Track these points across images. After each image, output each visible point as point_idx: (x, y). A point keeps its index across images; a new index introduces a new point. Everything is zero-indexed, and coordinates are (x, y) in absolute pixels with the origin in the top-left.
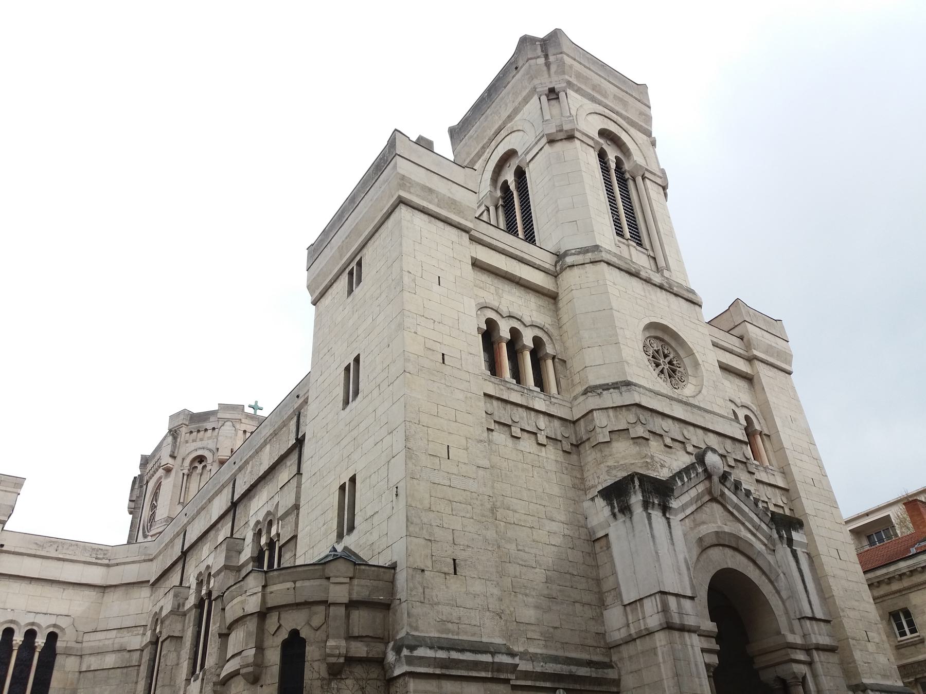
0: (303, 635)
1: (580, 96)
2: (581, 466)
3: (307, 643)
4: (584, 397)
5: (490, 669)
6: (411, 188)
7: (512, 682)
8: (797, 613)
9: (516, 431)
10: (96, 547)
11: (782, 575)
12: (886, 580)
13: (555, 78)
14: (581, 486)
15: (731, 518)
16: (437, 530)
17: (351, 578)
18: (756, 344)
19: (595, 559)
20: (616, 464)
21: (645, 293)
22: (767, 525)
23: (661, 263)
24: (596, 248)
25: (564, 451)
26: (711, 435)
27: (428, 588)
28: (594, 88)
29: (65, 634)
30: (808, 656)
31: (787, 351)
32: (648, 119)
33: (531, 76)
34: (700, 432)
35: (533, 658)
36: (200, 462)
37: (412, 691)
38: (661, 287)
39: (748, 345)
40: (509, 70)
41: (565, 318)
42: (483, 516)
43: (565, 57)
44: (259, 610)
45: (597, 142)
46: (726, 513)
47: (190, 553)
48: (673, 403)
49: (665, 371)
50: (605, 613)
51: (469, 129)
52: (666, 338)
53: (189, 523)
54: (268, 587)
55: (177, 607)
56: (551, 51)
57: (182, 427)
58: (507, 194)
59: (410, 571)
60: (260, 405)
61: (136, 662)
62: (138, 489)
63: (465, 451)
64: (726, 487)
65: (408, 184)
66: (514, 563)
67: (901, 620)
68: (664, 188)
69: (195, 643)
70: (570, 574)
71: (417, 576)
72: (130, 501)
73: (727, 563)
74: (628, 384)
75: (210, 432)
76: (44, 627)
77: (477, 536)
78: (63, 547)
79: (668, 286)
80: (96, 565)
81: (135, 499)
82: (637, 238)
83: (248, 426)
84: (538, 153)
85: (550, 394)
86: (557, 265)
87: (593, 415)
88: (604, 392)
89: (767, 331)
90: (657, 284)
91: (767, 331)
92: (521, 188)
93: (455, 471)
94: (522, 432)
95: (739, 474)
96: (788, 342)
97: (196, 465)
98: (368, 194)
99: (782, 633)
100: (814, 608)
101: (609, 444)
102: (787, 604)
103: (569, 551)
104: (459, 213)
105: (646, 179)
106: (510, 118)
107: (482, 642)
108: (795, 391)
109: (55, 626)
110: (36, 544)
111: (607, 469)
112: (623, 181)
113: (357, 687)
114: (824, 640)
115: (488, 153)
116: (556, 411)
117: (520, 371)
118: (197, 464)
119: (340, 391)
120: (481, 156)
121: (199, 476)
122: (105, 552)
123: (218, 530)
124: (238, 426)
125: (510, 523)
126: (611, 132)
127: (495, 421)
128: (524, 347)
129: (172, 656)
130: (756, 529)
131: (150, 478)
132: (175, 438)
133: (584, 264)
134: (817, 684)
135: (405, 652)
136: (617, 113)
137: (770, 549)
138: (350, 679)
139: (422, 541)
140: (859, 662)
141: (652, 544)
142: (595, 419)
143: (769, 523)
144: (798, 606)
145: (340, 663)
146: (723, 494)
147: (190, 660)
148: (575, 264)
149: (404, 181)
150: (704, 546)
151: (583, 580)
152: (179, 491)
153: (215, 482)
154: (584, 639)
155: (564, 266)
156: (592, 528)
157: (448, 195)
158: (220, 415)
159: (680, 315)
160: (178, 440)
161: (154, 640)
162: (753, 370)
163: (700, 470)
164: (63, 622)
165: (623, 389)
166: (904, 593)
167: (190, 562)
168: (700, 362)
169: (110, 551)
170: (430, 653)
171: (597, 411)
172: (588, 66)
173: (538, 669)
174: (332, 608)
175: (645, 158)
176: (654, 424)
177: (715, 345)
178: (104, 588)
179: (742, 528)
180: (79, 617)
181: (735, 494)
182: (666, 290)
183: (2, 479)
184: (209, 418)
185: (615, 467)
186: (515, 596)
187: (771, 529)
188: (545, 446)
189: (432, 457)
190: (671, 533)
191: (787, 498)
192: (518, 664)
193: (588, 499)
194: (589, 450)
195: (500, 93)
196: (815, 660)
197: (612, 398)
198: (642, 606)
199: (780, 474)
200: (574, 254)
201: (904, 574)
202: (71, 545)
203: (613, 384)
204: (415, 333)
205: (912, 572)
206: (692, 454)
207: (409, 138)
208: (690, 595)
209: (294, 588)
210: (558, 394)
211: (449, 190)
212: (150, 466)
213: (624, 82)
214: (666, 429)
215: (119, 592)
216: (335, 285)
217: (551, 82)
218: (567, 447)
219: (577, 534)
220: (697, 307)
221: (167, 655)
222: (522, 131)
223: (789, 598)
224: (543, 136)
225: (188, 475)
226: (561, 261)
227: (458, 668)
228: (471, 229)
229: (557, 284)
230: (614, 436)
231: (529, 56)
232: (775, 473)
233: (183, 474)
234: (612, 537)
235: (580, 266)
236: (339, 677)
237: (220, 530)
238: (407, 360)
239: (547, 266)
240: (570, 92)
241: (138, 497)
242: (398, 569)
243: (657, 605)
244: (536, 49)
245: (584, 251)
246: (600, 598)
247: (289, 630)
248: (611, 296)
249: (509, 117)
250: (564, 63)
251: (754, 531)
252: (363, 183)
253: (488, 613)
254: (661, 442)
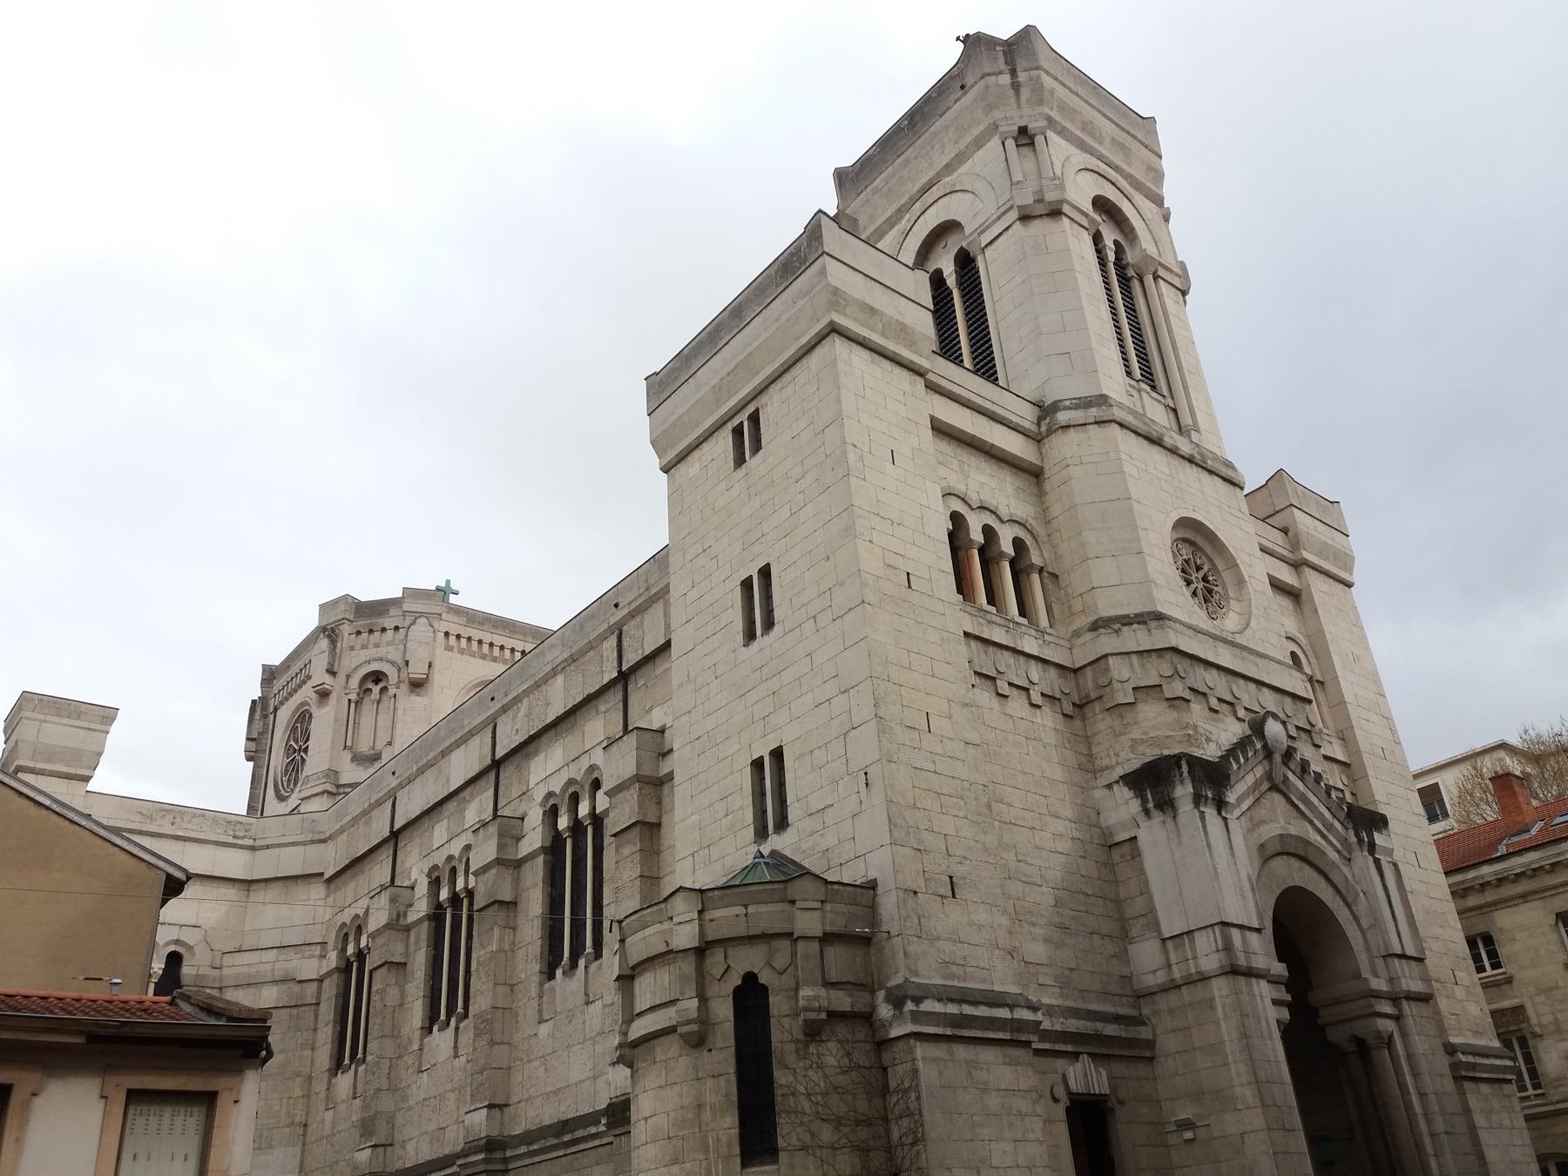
0: (763, 979)
1: (1064, 142)
2: (1087, 737)
3: (770, 992)
4: (1092, 635)
5: (1009, 1029)
6: (847, 308)
7: (1034, 1046)
8: (1382, 947)
9: (1003, 686)
10: (233, 818)
11: (1362, 895)
12: (1460, 891)
13: (1027, 110)
14: (1088, 766)
15: (1296, 814)
16: (926, 835)
17: (822, 902)
18: (1306, 541)
19: (1113, 872)
20: (1143, 737)
21: (1170, 470)
22: (1342, 823)
23: (1186, 420)
24: (1103, 400)
25: (1065, 715)
26: (1266, 691)
27: (924, 916)
29: (194, 954)
30: (1395, 1007)
31: (1347, 552)
32: (1159, 176)
33: (990, 105)
34: (1252, 686)
35: (1050, 1011)
36: (377, 682)
37: (920, 1059)
38: (1191, 460)
39: (1295, 544)
40: (948, 89)
41: (1056, 509)
42: (979, 814)
43: (1044, 76)
44: (697, 945)
45: (1092, 221)
46: (1289, 807)
47: (406, 834)
48: (1219, 644)
49: (1199, 592)
50: (1130, 947)
51: (874, 176)
52: (1199, 541)
53: (401, 786)
54: (706, 913)
55: (395, 917)
56: (1021, 64)
57: (344, 623)
58: (940, 292)
59: (901, 893)
60: (454, 586)
61: (312, 998)
62: (260, 720)
63: (948, 720)
64: (1290, 769)
65: (842, 302)
66: (1015, 878)
67: (1479, 949)
68: (1184, 293)
69: (431, 973)
70: (1084, 893)
71: (910, 900)
72: (248, 739)
73: (1293, 878)
74: (1159, 617)
75: (390, 633)
76: (161, 944)
77: (974, 843)
78: (183, 819)
79: (1199, 458)
80: (234, 847)
81: (255, 736)
82: (1148, 376)
83: (452, 625)
84: (1001, 234)
85: (1038, 627)
86: (1042, 423)
87: (1107, 663)
88: (1125, 629)
89: (1321, 521)
91: (1321, 521)
92: (965, 285)
93: (939, 749)
94: (1011, 688)
95: (1304, 751)
96: (1348, 536)
97: (370, 687)
98: (769, 308)
99: (1364, 976)
100: (1404, 940)
101: (1133, 706)
102: (1369, 936)
103: (1081, 861)
104: (910, 345)
105: (1160, 280)
106: (949, 168)
107: (993, 991)
108: (1357, 615)
109: (177, 942)
110: (141, 813)
111: (1130, 744)
112: (1125, 281)
113: (842, 1052)
114: (1416, 986)
115: (908, 221)
116: (1051, 654)
118: (370, 686)
119: (736, 616)
120: (895, 224)
121: (375, 704)
122: (247, 827)
123: (465, 801)
124: (436, 625)
125: (1006, 823)
126: (1108, 201)
127: (975, 672)
128: (1002, 554)
129: (393, 995)
131: (282, 703)
132: (333, 642)
133: (1085, 424)
134: (1406, 1046)
135: (910, 1006)
136: (1117, 169)
137: (1345, 858)
138: (833, 1041)
139: (909, 852)
140: (1446, 1014)
141: (1207, 854)
142: (1112, 668)
144: (1383, 938)
145: (821, 1020)
146: (1286, 779)
147: (426, 999)
148: (1072, 423)
149: (837, 298)
150: (1267, 854)
151: (1100, 902)
152: (344, 728)
153: (454, 725)
154: (1107, 984)
155: (1055, 427)
156: (1108, 827)
157: (896, 317)
158: (407, 607)
159: (1217, 503)
160: (339, 645)
161: (343, 965)
162: (1300, 581)
163: (1259, 746)
164: (190, 937)
165: (1153, 624)
166: (1485, 910)
167: (408, 848)
168: (1247, 579)
169: (254, 826)
170: (937, 1007)
171: (1114, 657)
172: (1075, 90)
173: (1058, 1027)
174: (801, 945)
175: (1156, 243)
176: (1196, 678)
177: (1263, 550)
178: (248, 884)
179: (1309, 828)
180: (212, 928)
181: (1301, 779)
182: (1197, 465)
183: (82, 710)
184: (388, 610)
185: (1143, 741)
186: (1020, 926)
187: (1347, 829)
188: (1039, 707)
189: (909, 730)
190: (1229, 838)
191: (1348, 777)
192: (1041, 1022)
193: (1100, 785)
194: (1101, 712)
195: (931, 123)
196: (1405, 1013)
197: (1136, 638)
198: (1192, 941)
199: (1338, 741)
200: (1070, 408)
201: (1488, 883)
202: (195, 816)
203: (1137, 615)
204: (871, 542)
205: (1501, 881)
206: (1244, 721)
207: (840, 227)
208: (1257, 927)
209: (746, 915)
210: (1050, 627)
211: (896, 307)
212: (278, 684)
213: (1125, 115)
214: (1211, 685)
215: (273, 892)
216: (706, 447)
217: (1022, 117)
218: (1069, 709)
219: (1088, 836)
220: (1238, 490)
221: (384, 990)
222: (971, 192)
223: (1371, 926)
224: (1011, 207)
225: (357, 703)
226: (1048, 418)
227: (971, 1028)
228: (928, 371)
229: (1041, 453)
230: (1139, 695)
231: (987, 70)
232: (1332, 740)
233: (349, 700)
234: (1144, 842)
235: (1079, 428)
236: (818, 1039)
237: (468, 801)
238: (864, 585)
239: (1027, 425)
240: (1051, 134)
241: (260, 734)
242: (880, 890)
243: (1216, 941)
244: (996, 59)
245: (1085, 403)
246: (1122, 928)
247: (742, 973)
248: (1128, 477)
249: (947, 166)
250: (1043, 86)
252: (758, 288)
253: (997, 951)
254: (1205, 704)
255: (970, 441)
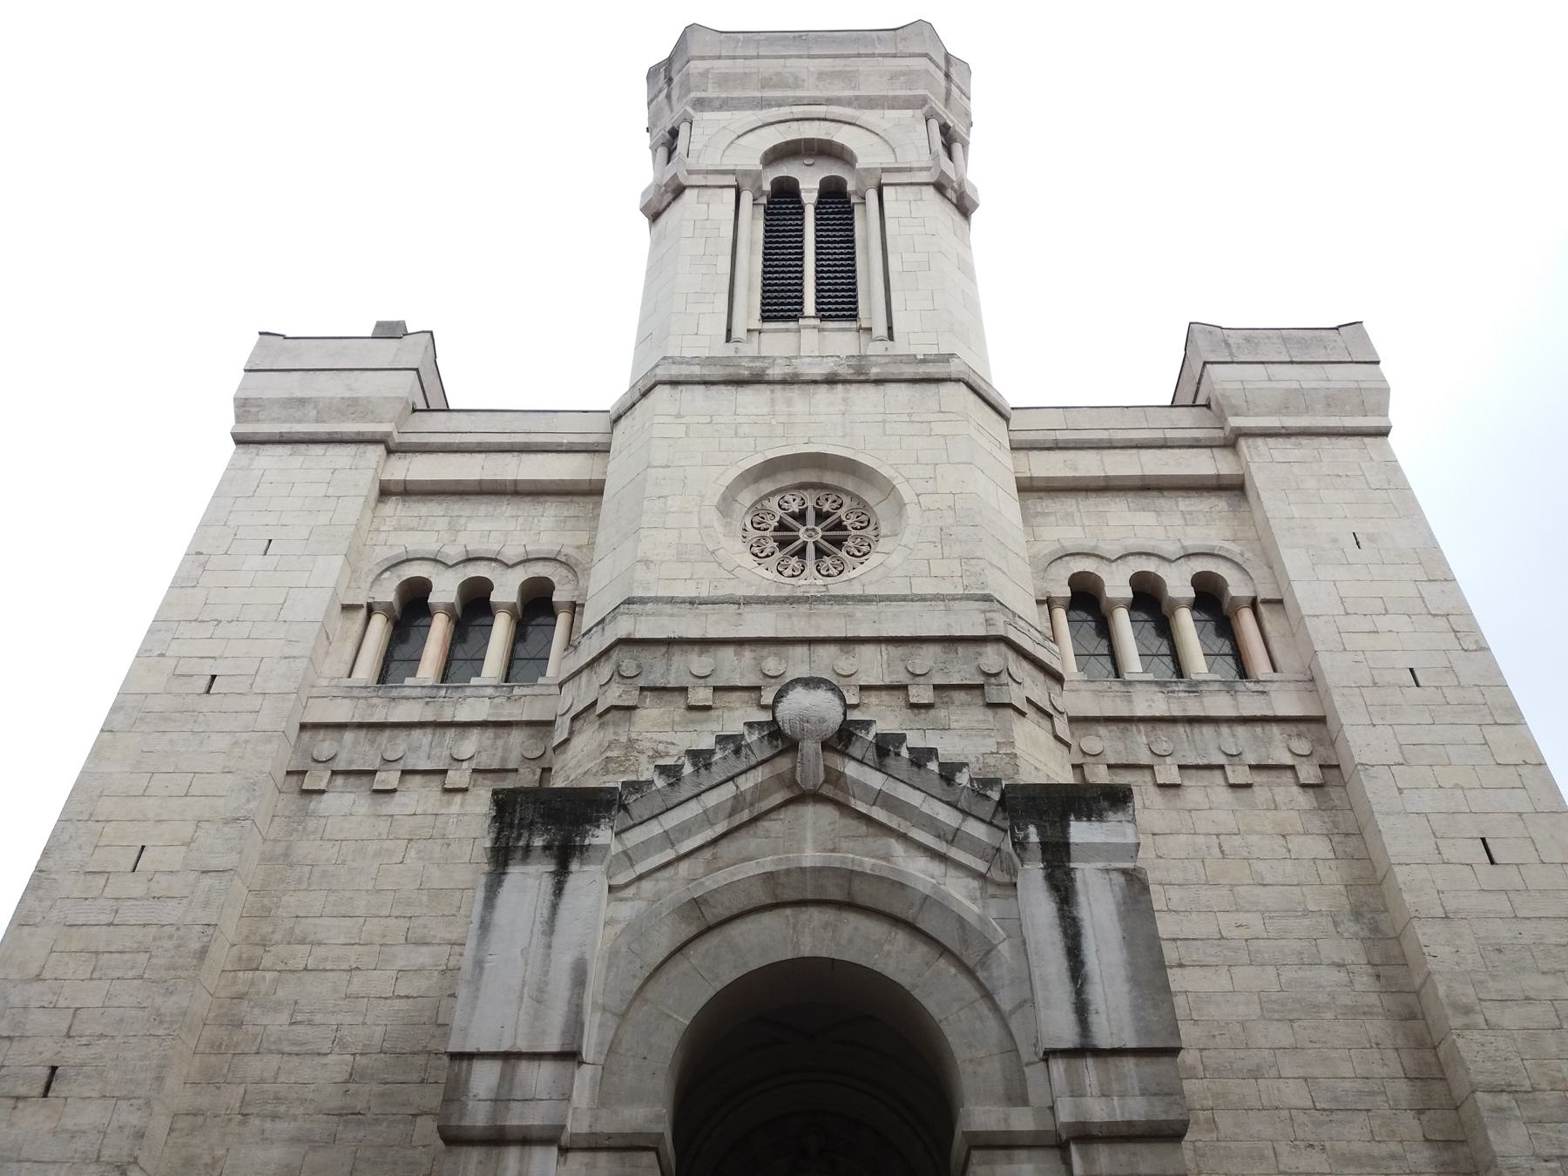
28: (765, 84)
52: (829, 478)
79: (851, 371)
90: (818, 378)
117: (1242, 651)
128: (1114, 604)
130: (947, 842)
136: (829, 101)
143: (994, 816)
181: (880, 768)
190: (554, 907)
251: (941, 847)
255: (478, 489)
